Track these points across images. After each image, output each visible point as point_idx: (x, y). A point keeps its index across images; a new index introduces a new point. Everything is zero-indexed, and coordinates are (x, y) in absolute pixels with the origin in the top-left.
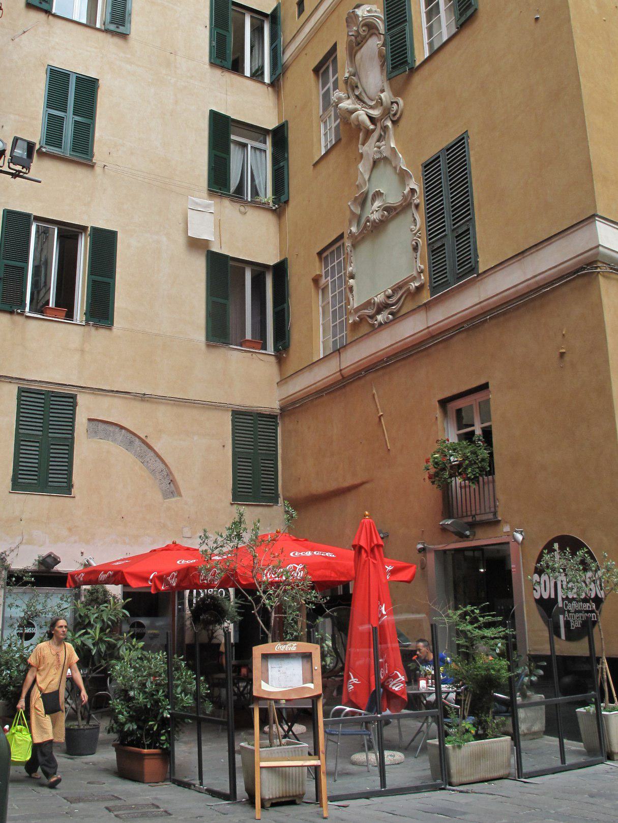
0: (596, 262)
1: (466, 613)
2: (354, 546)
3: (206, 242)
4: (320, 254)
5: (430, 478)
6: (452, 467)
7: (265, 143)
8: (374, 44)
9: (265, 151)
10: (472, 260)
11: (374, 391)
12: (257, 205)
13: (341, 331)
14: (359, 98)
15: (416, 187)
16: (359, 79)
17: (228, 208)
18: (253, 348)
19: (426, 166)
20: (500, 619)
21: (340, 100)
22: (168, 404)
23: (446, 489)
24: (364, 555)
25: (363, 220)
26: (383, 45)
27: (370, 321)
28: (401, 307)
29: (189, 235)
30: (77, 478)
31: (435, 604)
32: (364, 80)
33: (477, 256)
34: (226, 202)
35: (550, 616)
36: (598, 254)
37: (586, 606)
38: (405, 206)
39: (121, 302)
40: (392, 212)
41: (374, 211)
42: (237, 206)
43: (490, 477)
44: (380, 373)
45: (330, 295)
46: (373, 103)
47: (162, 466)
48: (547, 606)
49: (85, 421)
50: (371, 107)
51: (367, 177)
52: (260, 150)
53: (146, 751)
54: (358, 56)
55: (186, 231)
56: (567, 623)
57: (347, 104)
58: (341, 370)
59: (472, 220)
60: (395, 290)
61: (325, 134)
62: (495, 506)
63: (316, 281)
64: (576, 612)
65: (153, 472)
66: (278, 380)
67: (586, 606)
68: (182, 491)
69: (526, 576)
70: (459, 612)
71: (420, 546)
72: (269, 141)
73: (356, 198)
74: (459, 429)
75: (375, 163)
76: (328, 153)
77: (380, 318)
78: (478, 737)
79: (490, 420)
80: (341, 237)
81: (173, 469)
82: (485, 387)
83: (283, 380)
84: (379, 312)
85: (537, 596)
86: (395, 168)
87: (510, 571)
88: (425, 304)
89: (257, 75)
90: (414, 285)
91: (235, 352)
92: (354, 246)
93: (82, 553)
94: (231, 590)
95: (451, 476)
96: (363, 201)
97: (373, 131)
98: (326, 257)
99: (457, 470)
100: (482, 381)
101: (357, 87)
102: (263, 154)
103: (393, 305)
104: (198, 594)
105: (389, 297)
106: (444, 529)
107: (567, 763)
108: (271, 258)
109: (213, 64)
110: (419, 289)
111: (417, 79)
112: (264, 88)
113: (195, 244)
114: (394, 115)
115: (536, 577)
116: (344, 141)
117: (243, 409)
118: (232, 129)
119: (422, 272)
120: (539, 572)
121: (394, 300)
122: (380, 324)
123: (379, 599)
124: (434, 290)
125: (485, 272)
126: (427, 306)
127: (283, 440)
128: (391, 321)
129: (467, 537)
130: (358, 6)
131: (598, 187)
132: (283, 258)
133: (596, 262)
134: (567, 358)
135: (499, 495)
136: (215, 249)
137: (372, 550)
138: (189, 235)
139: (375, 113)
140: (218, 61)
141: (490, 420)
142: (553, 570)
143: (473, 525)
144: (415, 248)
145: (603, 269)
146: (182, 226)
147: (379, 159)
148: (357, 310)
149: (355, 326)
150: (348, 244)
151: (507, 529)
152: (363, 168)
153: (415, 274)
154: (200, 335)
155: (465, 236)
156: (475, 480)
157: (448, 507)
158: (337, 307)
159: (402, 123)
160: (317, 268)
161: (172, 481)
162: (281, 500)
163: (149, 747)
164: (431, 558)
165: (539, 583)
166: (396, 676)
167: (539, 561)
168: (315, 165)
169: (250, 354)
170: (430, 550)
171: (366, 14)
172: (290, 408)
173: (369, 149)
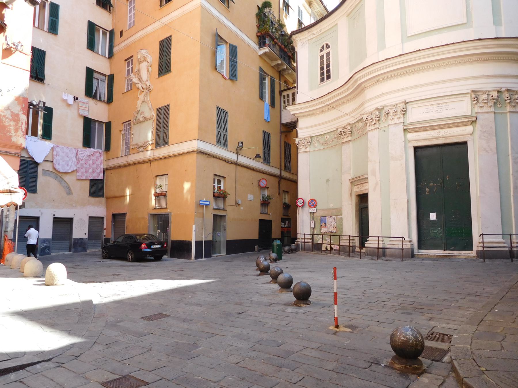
25: (137, 119)
30: (38, 188)
39: (54, 132)
49: (41, 170)
65: (64, 187)
93: (40, 211)
102: (104, 83)
107: (88, 107)
139: (144, 86)
154: (81, 144)
155: (166, 134)
159: (152, 92)
162: (104, 196)
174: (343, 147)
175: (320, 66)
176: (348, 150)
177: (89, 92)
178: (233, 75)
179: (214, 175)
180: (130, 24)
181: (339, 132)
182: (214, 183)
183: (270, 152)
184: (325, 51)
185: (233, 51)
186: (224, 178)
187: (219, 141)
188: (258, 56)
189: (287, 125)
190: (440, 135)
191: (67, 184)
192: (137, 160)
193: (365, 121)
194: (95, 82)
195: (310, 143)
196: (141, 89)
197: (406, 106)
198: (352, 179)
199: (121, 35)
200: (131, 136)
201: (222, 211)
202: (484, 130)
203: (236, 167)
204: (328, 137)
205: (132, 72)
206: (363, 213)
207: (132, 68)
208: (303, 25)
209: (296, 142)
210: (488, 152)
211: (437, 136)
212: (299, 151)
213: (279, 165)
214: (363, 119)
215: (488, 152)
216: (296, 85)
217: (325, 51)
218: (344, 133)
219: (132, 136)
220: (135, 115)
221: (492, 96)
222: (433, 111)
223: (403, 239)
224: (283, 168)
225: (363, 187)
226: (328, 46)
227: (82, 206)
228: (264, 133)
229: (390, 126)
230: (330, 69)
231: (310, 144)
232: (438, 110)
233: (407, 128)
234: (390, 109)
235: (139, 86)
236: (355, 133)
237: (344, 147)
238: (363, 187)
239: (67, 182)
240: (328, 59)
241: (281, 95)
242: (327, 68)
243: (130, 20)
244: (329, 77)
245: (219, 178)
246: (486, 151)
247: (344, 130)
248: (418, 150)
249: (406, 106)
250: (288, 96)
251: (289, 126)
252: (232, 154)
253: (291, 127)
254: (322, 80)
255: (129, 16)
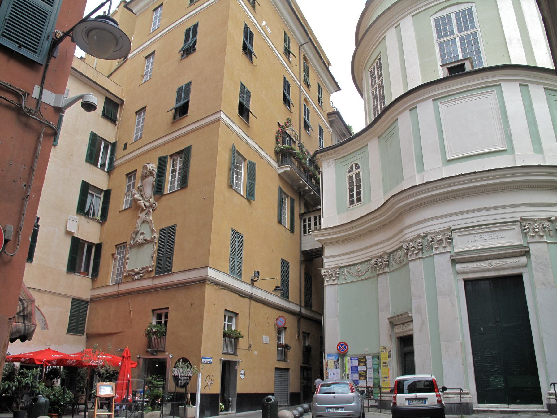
0: (206, 280)
1: (153, 378)
2: (122, 356)
3: (72, 233)
4: (116, 246)
5: (145, 335)
6: (153, 332)
7: (101, 194)
8: (151, 180)
9: (100, 198)
10: (170, 267)
11: (130, 301)
12: (93, 219)
13: (120, 276)
14: (142, 195)
15: (156, 236)
16: (143, 189)
17: (83, 219)
18: (84, 275)
19: (161, 230)
20: (163, 379)
21: (135, 194)
22: (48, 294)
23: (150, 339)
24: (125, 359)
25: (135, 240)
26: (154, 182)
27: (132, 277)
28: (144, 275)
29: (67, 229)
31: (145, 374)
32: (145, 190)
33: (172, 266)
34: (83, 217)
35: (176, 380)
36: (207, 278)
37: (187, 378)
38: (151, 241)
40: (146, 242)
41: (140, 239)
42: (87, 219)
43: (165, 337)
44: (133, 295)
45: (118, 262)
46: (147, 200)
47: (42, 318)
48: (176, 378)
50: (146, 201)
51: (139, 225)
52: (98, 197)
53: (54, 414)
54: (145, 180)
55: (66, 227)
56: (181, 383)
57: (137, 196)
58: (118, 291)
59: (172, 254)
60: (143, 269)
61: (126, 201)
62: (165, 346)
63: (113, 255)
64: (184, 380)
66: (91, 288)
67: (187, 378)
68: (49, 328)
69: (171, 368)
70: (152, 377)
71: (138, 356)
72: (103, 194)
73: (134, 232)
74: (157, 320)
75: (143, 222)
76: (126, 210)
77: (136, 277)
78: (152, 411)
79: (167, 319)
80: (126, 242)
81: (47, 319)
82: (168, 308)
83: (93, 289)
84: (136, 274)
85: (173, 375)
86: (150, 227)
87: (166, 367)
88: (153, 277)
89: (103, 166)
90: (150, 269)
91: (77, 276)
92: (130, 248)
94: (62, 367)
95: (152, 335)
96: (137, 233)
97: (145, 210)
98: (118, 247)
99: (155, 333)
100: (167, 307)
101: (142, 191)
102: (99, 199)
103: (141, 274)
104: (49, 367)
105: (140, 271)
106: (147, 352)
108: (96, 241)
109: (87, 161)
110: (151, 271)
111: (164, 198)
112: (105, 173)
113: (68, 233)
114: (154, 208)
115: (174, 369)
116: (133, 208)
117: (76, 298)
118: (90, 187)
119: (153, 265)
120: (175, 367)
121: (142, 272)
122: (136, 279)
123: (128, 372)
124: (156, 273)
125: (174, 273)
126: (153, 278)
127: (89, 311)
128: (140, 279)
129: (155, 355)
130: (148, 164)
131: (211, 257)
132: (100, 242)
133: (206, 280)
134: (193, 306)
135: (166, 343)
136: (75, 235)
137: (128, 358)
138: (67, 229)
139: (147, 204)
140: (89, 160)
141: (167, 319)
142: (179, 367)
143: (157, 351)
144: (152, 257)
145: (208, 282)
146: (64, 225)
147: (145, 221)
148: (128, 272)
149: (126, 277)
150: (128, 247)
151: (167, 353)
152: (139, 222)
153: (151, 265)
154: (65, 269)
155: (170, 257)
156: (160, 338)
157: (149, 345)
158: (120, 267)
159: (155, 211)
160: (114, 251)
161: (46, 324)
162: (85, 333)
163: (54, 413)
164: (141, 361)
165: (174, 371)
166: (130, 395)
167: (175, 364)
168: (120, 212)
169: (82, 277)
170: (141, 358)
171: (151, 168)
172: (94, 300)
173: (142, 215)
174: (379, 279)
175: (349, 187)
176: (385, 282)
177: (82, 209)
178: (251, 194)
179: (226, 310)
180: (136, 137)
181: (373, 262)
182: (225, 321)
183: (289, 284)
184: (355, 172)
185: (252, 168)
186: (236, 314)
187: (232, 270)
188: (277, 176)
189: (308, 253)
190: (492, 267)
191: (43, 316)
192: (183, 280)
193: (406, 249)
194: (89, 198)
195: (338, 274)
196: (144, 206)
197: (452, 233)
198: (392, 318)
199: (125, 148)
200: (126, 260)
201: (233, 356)
202: (539, 261)
203: (250, 301)
204: (359, 266)
205: (133, 188)
206: (406, 359)
207: (134, 183)
208: (250, 113)
209: (322, 273)
210: (546, 286)
211: (489, 267)
212: (326, 283)
213: (298, 300)
214: (403, 247)
215: (546, 286)
216: (320, 207)
217: (355, 172)
218: (380, 263)
219: (127, 261)
220: (133, 236)
221: (543, 225)
222: (482, 239)
223: (460, 391)
224: (303, 304)
225: (406, 327)
226: (357, 166)
227: (57, 345)
228: (283, 261)
229: (435, 256)
230: (361, 191)
231: (338, 275)
232: (486, 239)
233: (455, 258)
234: (434, 236)
235: (142, 202)
236: (392, 263)
237: (380, 278)
238: (406, 327)
239: (44, 314)
240: (358, 181)
241: (300, 219)
242: (357, 190)
243: (137, 132)
244: (359, 200)
245: (231, 315)
246: (544, 285)
247: (380, 260)
248: (469, 283)
249: (452, 233)
250: (310, 220)
251: (310, 255)
252: (246, 285)
253: (313, 255)
254: (352, 202)
255: (136, 128)
